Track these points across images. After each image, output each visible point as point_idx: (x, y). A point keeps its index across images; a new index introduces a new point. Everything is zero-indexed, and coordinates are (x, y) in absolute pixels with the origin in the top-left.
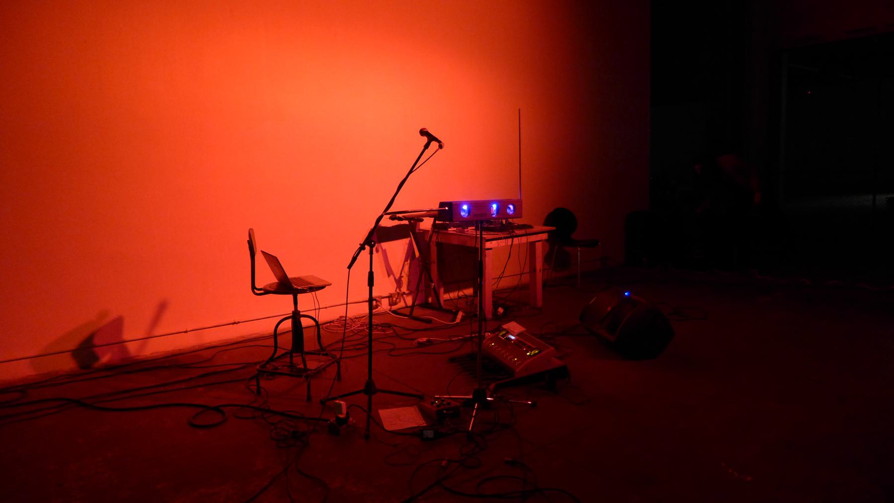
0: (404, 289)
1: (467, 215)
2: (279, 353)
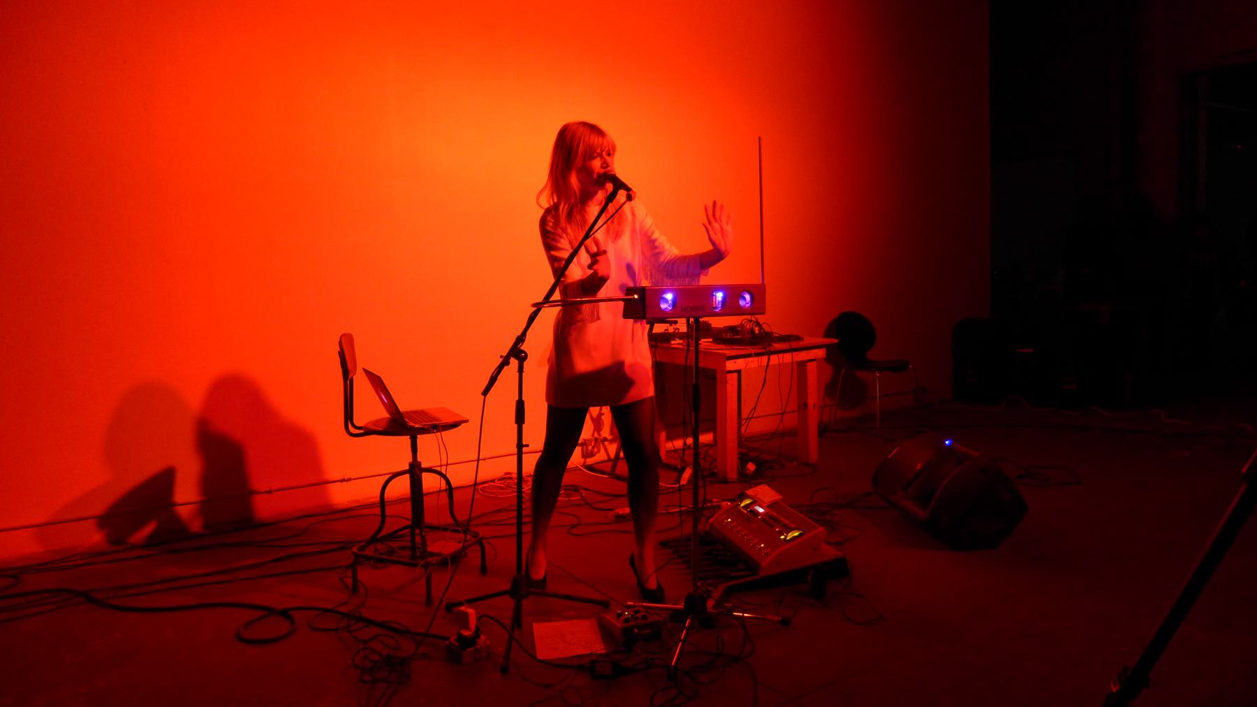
0: (606, 433)
2: (383, 533)
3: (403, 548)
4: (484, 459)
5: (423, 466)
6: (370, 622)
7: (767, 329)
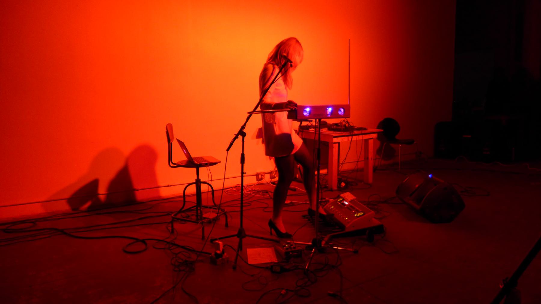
2: (185, 208)
5: (201, 181)
6: (178, 246)
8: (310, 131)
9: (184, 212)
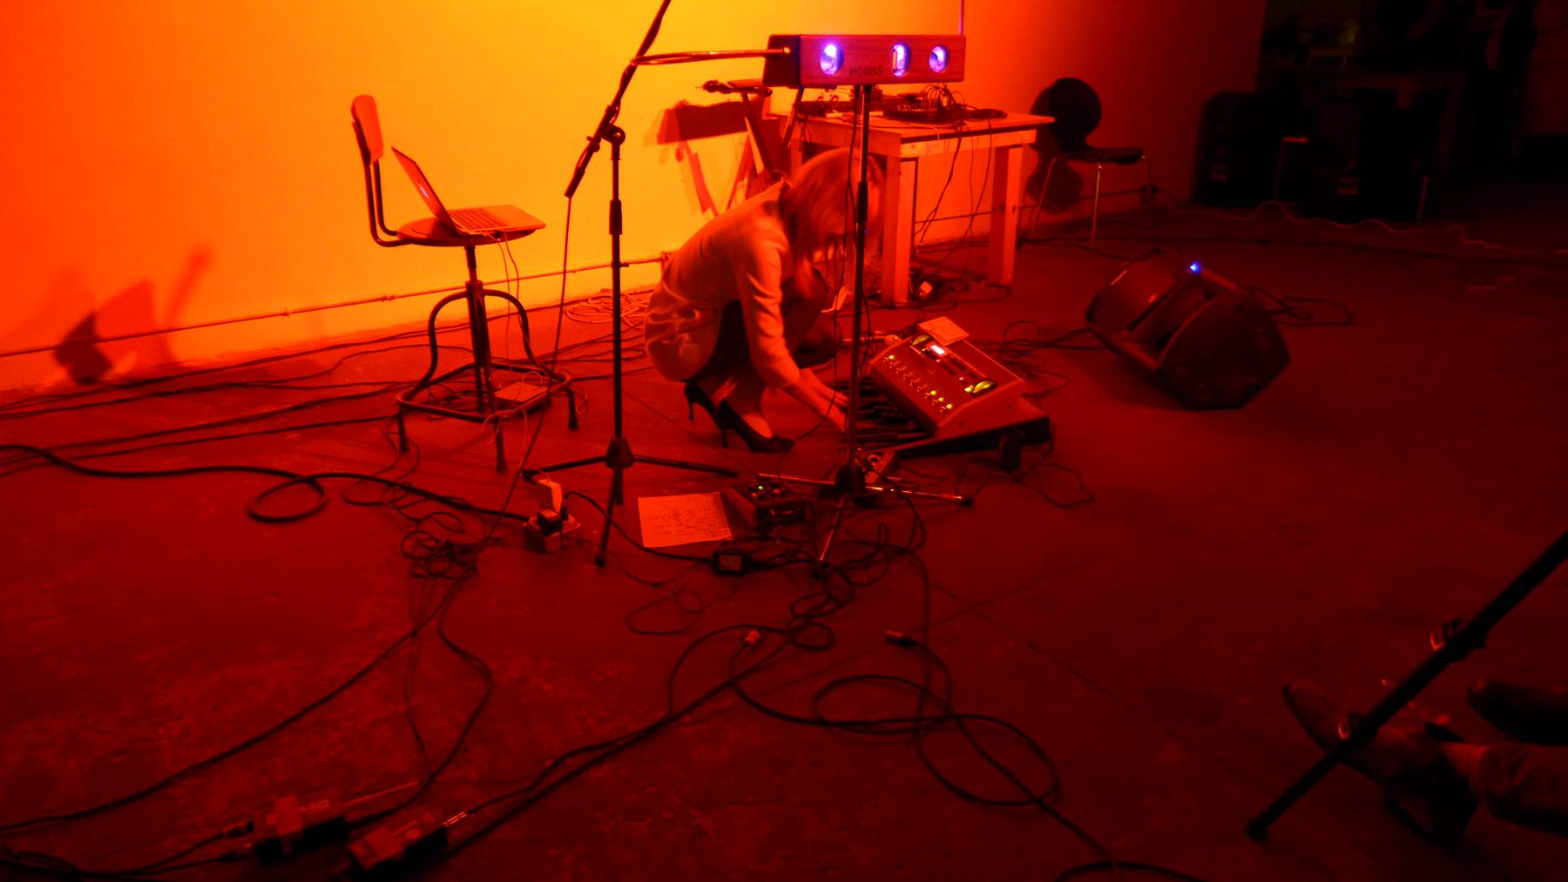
1: (835, 69)
2: (436, 376)
3: (466, 393)
4: (573, 272)
6: (428, 496)
7: (958, 99)
8: (828, 121)
9: (436, 382)
